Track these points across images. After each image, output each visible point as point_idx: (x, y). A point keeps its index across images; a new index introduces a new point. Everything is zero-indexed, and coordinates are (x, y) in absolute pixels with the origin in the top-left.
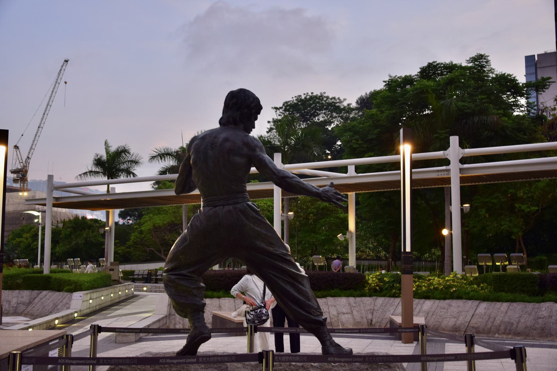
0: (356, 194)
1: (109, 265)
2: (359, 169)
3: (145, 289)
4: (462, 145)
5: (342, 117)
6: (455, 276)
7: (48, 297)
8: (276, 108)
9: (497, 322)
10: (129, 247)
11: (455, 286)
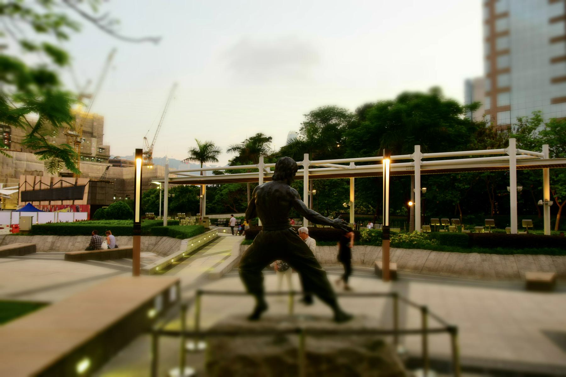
0: (355, 179)
1: (202, 218)
2: (357, 164)
3: (224, 231)
4: (423, 151)
5: (346, 121)
6: (416, 233)
7: (166, 242)
8: (306, 115)
10: (214, 204)
11: (416, 240)
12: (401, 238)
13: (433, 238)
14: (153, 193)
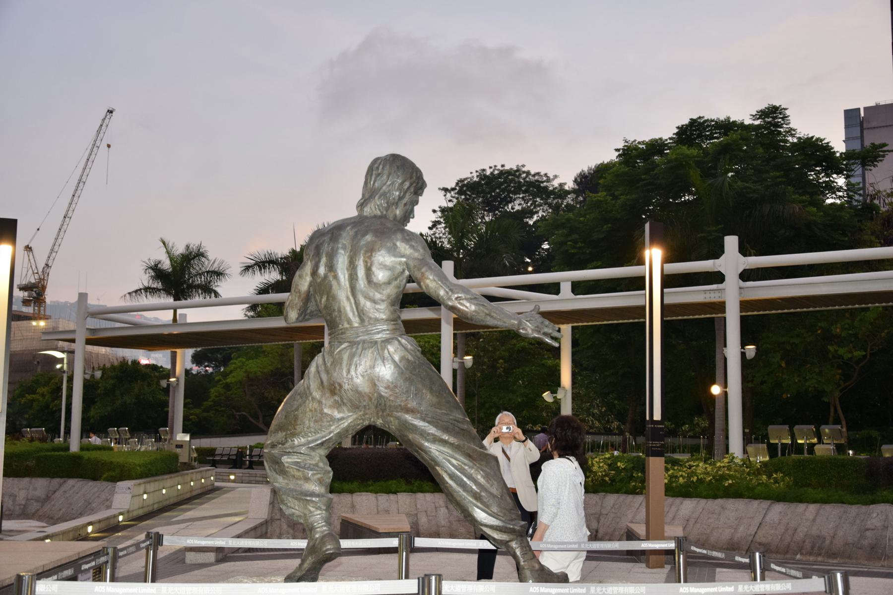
2: (579, 288)
5: (550, 206)
6: (732, 461)
7: (76, 489)
8: (446, 190)
9: (800, 536)
11: (731, 477)
12: (693, 473)
13: (776, 472)
14: (46, 384)
